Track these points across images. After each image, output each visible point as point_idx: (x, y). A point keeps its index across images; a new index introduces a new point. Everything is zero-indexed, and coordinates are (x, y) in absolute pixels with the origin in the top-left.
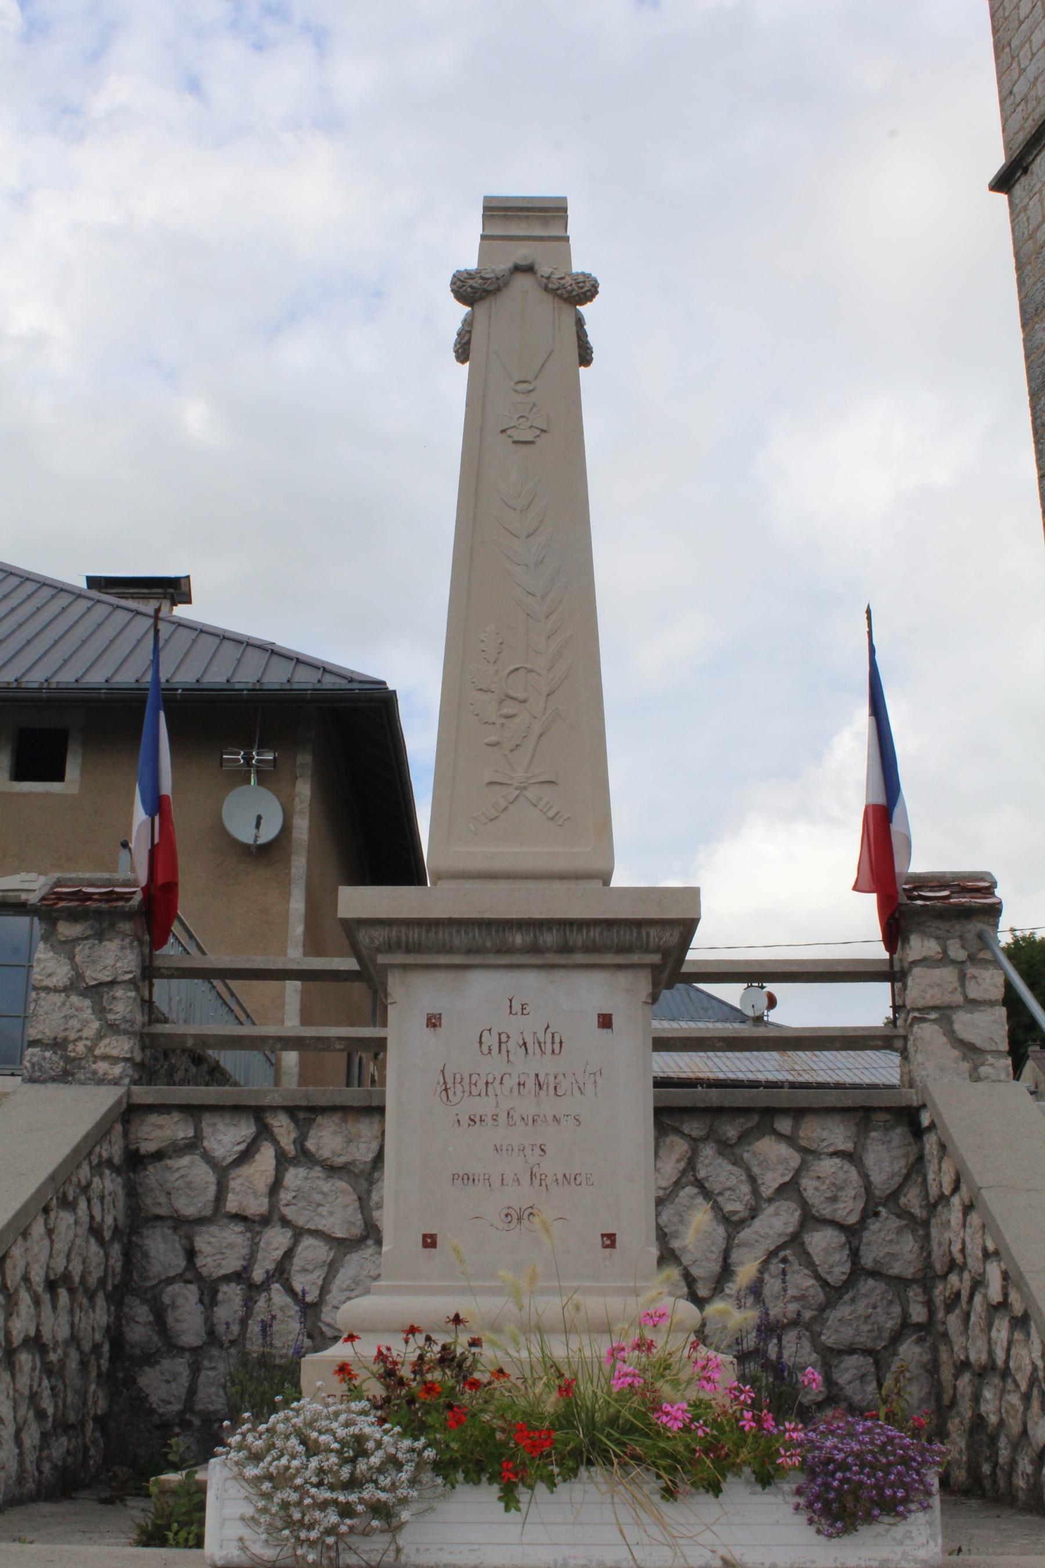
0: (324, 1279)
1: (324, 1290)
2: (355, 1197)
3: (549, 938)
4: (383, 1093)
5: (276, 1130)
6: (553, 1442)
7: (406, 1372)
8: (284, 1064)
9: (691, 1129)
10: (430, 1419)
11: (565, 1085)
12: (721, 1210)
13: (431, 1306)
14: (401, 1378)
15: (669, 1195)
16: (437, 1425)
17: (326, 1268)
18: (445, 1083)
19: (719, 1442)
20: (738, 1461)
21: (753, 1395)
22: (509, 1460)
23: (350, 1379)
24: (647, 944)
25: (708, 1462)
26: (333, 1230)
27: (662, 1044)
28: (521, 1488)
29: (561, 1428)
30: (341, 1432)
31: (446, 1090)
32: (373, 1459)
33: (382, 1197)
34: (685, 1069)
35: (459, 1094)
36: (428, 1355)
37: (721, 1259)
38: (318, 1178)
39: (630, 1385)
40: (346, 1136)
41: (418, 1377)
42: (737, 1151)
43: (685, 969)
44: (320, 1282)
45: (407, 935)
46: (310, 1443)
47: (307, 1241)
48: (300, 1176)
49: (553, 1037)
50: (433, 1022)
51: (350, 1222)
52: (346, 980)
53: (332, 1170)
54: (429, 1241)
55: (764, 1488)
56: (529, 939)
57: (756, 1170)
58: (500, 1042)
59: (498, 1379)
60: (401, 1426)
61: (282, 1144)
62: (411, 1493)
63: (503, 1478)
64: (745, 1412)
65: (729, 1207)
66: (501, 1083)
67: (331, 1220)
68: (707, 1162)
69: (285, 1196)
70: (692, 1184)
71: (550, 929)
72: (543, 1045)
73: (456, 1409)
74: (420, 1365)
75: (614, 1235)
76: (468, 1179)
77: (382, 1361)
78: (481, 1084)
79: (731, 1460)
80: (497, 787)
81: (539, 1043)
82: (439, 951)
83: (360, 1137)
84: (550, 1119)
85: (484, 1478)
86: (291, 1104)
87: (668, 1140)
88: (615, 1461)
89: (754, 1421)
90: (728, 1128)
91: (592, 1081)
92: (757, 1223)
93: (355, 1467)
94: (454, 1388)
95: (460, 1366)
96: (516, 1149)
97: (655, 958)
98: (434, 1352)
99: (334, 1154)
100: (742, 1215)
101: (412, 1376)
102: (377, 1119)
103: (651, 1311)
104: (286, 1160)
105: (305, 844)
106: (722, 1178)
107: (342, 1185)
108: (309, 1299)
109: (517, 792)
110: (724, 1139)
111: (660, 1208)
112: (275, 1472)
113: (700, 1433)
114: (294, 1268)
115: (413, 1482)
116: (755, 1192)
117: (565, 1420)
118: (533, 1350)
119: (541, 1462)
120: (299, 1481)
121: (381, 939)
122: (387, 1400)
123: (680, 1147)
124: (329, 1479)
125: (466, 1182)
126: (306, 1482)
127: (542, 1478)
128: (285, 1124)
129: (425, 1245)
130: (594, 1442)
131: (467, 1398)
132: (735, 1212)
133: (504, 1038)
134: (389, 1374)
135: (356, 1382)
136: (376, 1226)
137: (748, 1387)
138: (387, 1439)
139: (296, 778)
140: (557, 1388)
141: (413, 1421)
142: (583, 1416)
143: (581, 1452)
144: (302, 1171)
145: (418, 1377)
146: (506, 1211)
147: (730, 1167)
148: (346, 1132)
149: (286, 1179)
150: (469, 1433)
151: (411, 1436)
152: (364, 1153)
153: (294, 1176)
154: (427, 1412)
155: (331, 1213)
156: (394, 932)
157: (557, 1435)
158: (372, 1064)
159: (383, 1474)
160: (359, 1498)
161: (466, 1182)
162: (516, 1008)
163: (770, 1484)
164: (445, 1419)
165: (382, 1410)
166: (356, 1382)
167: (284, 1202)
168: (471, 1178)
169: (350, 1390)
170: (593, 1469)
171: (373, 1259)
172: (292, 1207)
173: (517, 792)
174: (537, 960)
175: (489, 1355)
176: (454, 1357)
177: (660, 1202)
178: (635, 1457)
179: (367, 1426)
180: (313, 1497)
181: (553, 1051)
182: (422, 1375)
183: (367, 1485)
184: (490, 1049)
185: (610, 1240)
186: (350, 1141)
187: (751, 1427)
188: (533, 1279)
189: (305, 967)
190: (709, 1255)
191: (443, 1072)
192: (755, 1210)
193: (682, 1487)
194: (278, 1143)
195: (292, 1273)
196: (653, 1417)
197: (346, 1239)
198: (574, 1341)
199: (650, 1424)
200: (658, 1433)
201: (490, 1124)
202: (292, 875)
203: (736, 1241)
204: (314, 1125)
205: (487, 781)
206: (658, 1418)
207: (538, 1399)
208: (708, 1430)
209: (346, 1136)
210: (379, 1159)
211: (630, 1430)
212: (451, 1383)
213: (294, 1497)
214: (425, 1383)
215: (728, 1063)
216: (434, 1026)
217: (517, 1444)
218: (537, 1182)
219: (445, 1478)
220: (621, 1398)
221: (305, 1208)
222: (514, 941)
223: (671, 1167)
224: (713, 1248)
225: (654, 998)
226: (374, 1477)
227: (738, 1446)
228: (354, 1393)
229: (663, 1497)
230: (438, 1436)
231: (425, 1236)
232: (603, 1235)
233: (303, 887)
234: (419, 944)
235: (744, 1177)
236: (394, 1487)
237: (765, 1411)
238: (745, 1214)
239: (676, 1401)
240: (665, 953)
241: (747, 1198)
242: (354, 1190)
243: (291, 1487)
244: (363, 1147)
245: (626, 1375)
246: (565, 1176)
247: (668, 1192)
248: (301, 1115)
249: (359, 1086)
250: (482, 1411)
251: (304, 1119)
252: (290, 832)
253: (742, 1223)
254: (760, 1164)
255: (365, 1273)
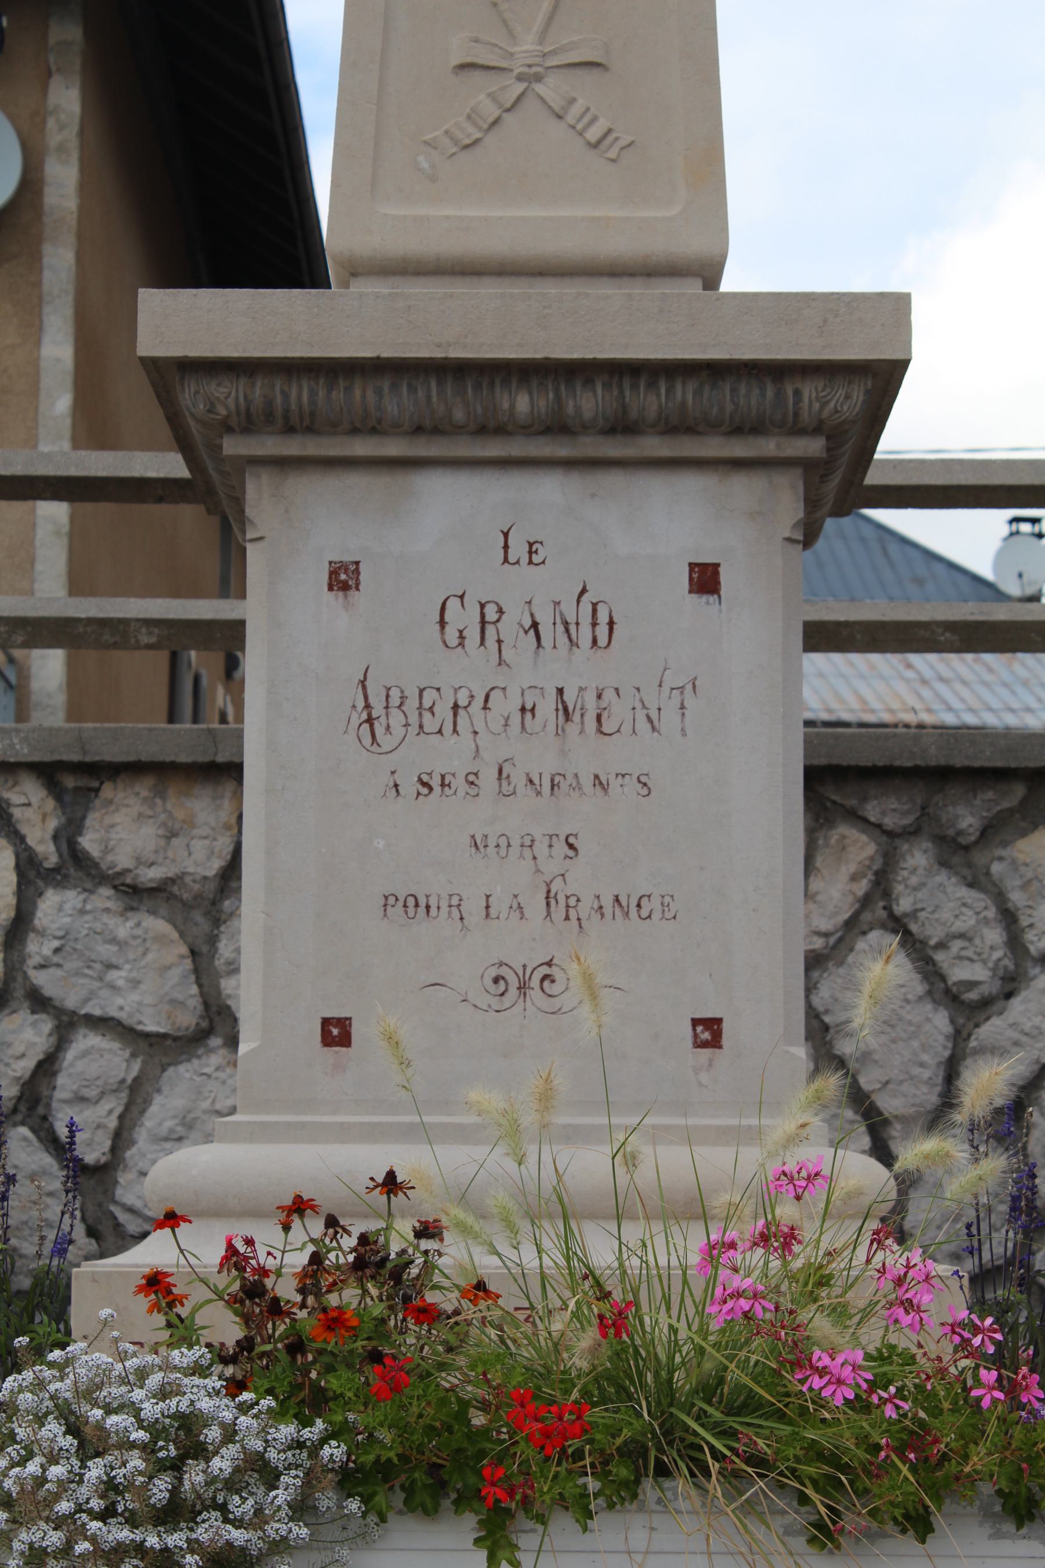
0: (121, 1117)
1: (121, 1139)
2: (184, 950)
3: (588, 402)
4: (239, 735)
5: (17, 813)
6: (586, 1429)
7: (286, 1290)
8: (35, 685)
9: (884, 813)
10: (333, 1383)
11: (619, 712)
12: (943, 978)
13: (338, 1164)
14: (276, 1300)
15: (834, 947)
16: (350, 1394)
17: (124, 1095)
18: (368, 706)
19: (928, 1432)
20: (967, 1469)
21: (998, 1336)
22: (500, 1459)
23: (171, 1305)
24: (796, 415)
25: (905, 1470)
26: (138, 1017)
27: (822, 637)
28: (523, 1521)
29: (604, 1400)
30: (151, 1410)
31: (370, 720)
32: (216, 1463)
33: (238, 951)
34: (876, 705)
35: (398, 731)
36: (332, 1256)
37: (940, 1080)
38: (107, 910)
39: (746, 1314)
40: (164, 824)
41: (311, 1300)
42: (979, 858)
43: (872, 478)
44: (113, 1123)
45: (285, 395)
46: (88, 1430)
47: (85, 1041)
48: (68, 907)
49: (594, 611)
50: (343, 579)
51: (173, 1001)
52: (160, 500)
53: (134, 894)
54: (335, 1032)
55: (1019, 1526)
56: (545, 402)
57: (1017, 898)
58: (483, 622)
59: (474, 1302)
60: (276, 1398)
61: (30, 841)
62: (295, 1530)
63: (482, 1499)
64: (983, 1372)
65: (958, 973)
66: (485, 708)
67: (135, 997)
68: (914, 880)
69: (37, 948)
70: (883, 926)
71: (589, 382)
72: (573, 629)
73: (387, 1362)
74: (314, 1275)
75: (719, 1021)
76: (416, 905)
77: (236, 1266)
78: (444, 710)
79: (952, 1467)
80: (477, 75)
81: (566, 624)
82: (354, 431)
83: (193, 826)
84: (587, 782)
85: (447, 1503)
86: (47, 758)
87: (834, 836)
88: (714, 1467)
89: (1001, 1388)
90: (960, 810)
91: (676, 702)
92: (1016, 1004)
93: (180, 1480)
94: (383, 1321)
95: (397, 1275)
96: (516, 842)
97: (813, 447)
98: (343, 1252)
99: (139, 861)
100: (985, 990)
101: (299, 1298)
102: (230, 786)
103: (791, 1167)
104: (39, 874)
105: (72, 220)
106: (946, 915)
107: (157, 925)
108: (90, 1157)
109: (521, 87)
110: (951, 832)
111: (815, 974)
112: (15, 1490)
113: (889, 1411)
114: (59, 1095)
115: (301, 1508)
116: (1015, 941)
117: (614, 1383)
118: (546, 1243)
119: (562, 1469)
120: (64, 1507)
121: (231, 402)
122: (246, 1345)
123: (860, 848)
124: (126, 1503)
125: (411, 911)
126: (79, 1509)
127: (562, 1503)
128: (34, 800)
129: (328, 1040)
130: (670, 1430)
131: (411, 1340)
132: (972, 985)
133: (491, 614)
134: (252, 1294)
135: (183, 1311)
136: (229, 1007)
137: (989, 1321)
138: (248, 1426)
139: (49, 74)
140: (596, 1321)
141: (300, 1387)
142: (649, 1378)
143: (644, 1452)
144: (72, 898)
145: (311, 1300)
146: (493, 972)
147: (964, 892)
148: (163, 816)
149: (39, 914)
150: (415, 1410)
151: (296, 1416)
152: (201, 861)
153: (55, 908)
154: (330, 1369)
155: (135, 983)
156: (258, 392)
157: (595, 1415)
158: (220, 691)
159: (238, 1492)
160: (188, 1541)
161: (411, 911)
162: (518, 550)
163: (1031, 1517)
164: (367, 1383)
165: (239, 1367)
166: (183, 1311)
167: (36, 960)
168: (423, 903)
169: (169, 1325)
170: (667, 1483)
171: (221, 1075)
172: (52, 971)
173: (521, 87)
174: (562, 449)
175: (455, 1256)
176: (386, 1259)
177: (814, 962)
178: (757, 1461)
179: (204, 1396)
180: (93, 1540)
181: (595, 641)
182: (318, 1295)
183: (205, 1515)
184: (462, 637)
185: (709, 1032)
186: (171, 835)
187: (995, 1401)
188: (546, 1098)
189: (73, 472)
190: (916, 1071)
191: (363, 683)
192: (1013, 979)
193: (849, 1521)
194: (22, 839)
195: (55, 1105)
196: (792, 1379)
197: (164, 1036)
198: (633, 1233)
199: (788, 1395)
200: (803, 1411)
201: (461, 793)
202: (46, 287)
203: (973, 1043)
204: (97, 802)
205: (456, 61)
206: (802, 1382)
207: (557, 1346)
208: (906, 1406)
209: (164, 824)
210: (232, 870)
211: (746, 1405)
212: (378, 1310)
213: (55, 1538)
214: (324, 1310)
215: (965, 693)
216: (345, 587)
217: (511, 1434)
218: (558, 912)
219: (366, 1500)
220: (730, 1345)
221: (78, 974)
222: (512, 406)
223: (839, 891)
224: (925, 1058)
225: (809, 534)
226: (220, 1499)
227: (973, 1435)
228: (182, 1332)
229: (812, 1540)
230: (351, 1417)
231: (326, 1022)
232: (695, 1022)
233: (69, 312)
234: (312, 414)
235: (991, 913)
236: (260, 1518)
237: (1025, 1370)
238: (993, 987)
239: (843, 1348)
240: (833, 433)
241: (997, 954)
242: (182, 935)
243: (47, 1520)
244: (199, 847)
245: (738, 1294)
246: (617, 899)
247: (832, 940)
248: (70, 782)
249: (195, 720)
250: (442, 1366)
251: (77, 789)
252: (39, 193)
253: (985, 1007)
254: (1025, 886)
255: (206, 1104)
